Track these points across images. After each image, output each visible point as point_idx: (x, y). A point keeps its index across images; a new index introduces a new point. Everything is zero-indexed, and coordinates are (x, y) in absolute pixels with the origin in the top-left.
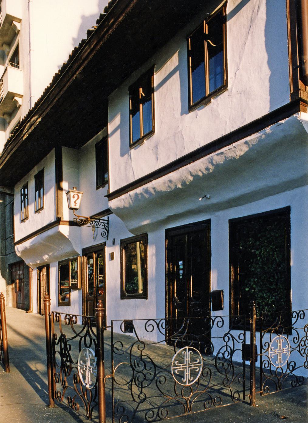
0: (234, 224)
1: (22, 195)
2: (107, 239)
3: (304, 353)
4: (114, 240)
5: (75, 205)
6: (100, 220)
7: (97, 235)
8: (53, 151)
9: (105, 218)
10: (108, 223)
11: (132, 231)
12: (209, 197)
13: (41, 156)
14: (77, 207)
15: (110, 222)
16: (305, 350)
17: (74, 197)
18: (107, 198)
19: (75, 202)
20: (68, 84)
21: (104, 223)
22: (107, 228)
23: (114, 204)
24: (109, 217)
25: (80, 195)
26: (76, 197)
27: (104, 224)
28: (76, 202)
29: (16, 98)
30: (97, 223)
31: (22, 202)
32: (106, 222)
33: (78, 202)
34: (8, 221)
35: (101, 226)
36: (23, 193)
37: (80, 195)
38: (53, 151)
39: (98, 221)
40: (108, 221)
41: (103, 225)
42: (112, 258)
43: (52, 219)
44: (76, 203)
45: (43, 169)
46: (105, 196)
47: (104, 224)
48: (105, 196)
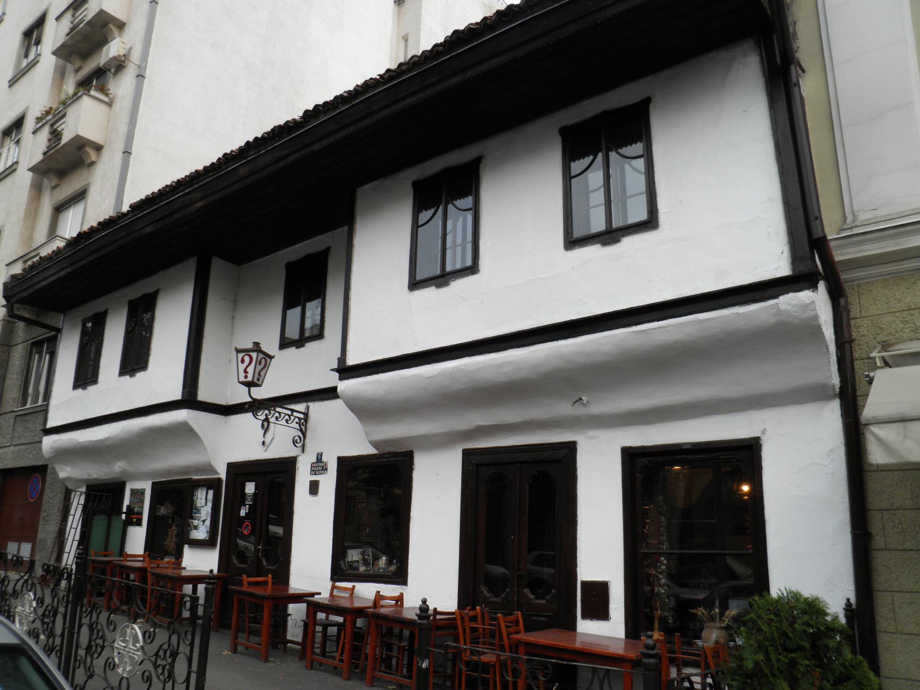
2: (303, 451)
3: (163, 673)
7: (273, 439)
9: (301, 407)
10: (306, 420)
11: (375, 444)
12: (585, 402)
15: (310, 424)
16: (164, 667)
17: (243, 361)
19: (245, 371)
20: (352, 129)
21: (299, 418)
22: (303, 428)
23: (346, 386)
24: (308, 408)
26: (247, 359)
30: (287, 417)
32: (302, 416)
33: (251, 370)
34: (15, 376)
39: (289, 412)
40: (306, 414)
42: (314, 488)
43: (176, 394)
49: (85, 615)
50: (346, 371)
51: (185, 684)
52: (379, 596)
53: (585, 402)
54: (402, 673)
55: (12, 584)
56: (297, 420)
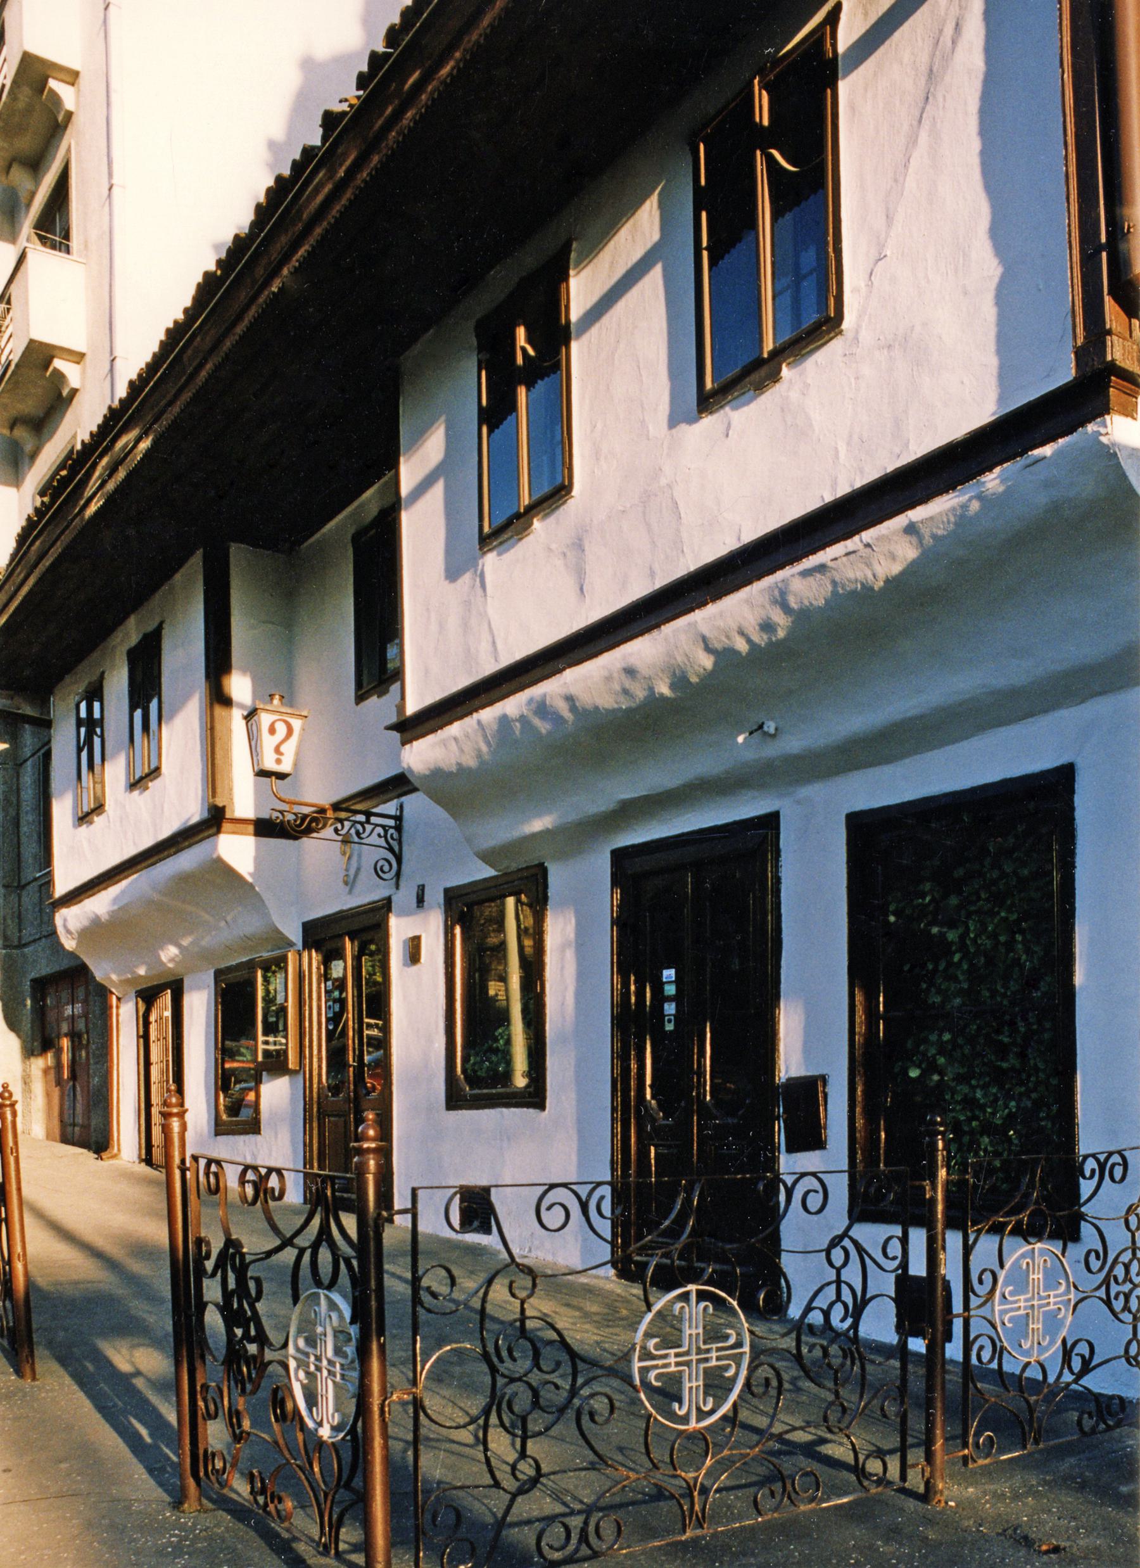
0: (867, 832)
1: (79, 723)
2: (397, 887)
4: (423, 891)
5: (278, 761)
6: (368, 814)
7: (358, 869)
8: (196, 562)
9: (390, 808)
10: (399, 828)
11: (487, 857)
12: (772, 731)
13: (147, 582)
14: (286, 767)
15: (406, 825)
17: (272, 731)
18: (396, 735)
19: (277, 750)
21: (383, 827)
23: (421, 755)
25: (297, 724)
26: (281, 729)
27: (386, 832)
28: (283, 749)
29: (58, 364)
31: (79, 750)
32: (392, 823)
33: (289, 748)
35: (374, 839)
36: (83, 714)
37: (297, 724)
38: (196, 562)
40: (399, 819)
41: (379, 835)
43: (193, 812)
44: (282, 754)
45: (160, 628)
46: (388, 728)
47: (386, 832)
48: (388, 728)
49: (1126, 1257)
50: (412, 727)
51: (814, 1305)
52: (504, 720)
53: (772, 731)
54: (249, 1523)
55: (683, 1474)
56: (380, 830)
